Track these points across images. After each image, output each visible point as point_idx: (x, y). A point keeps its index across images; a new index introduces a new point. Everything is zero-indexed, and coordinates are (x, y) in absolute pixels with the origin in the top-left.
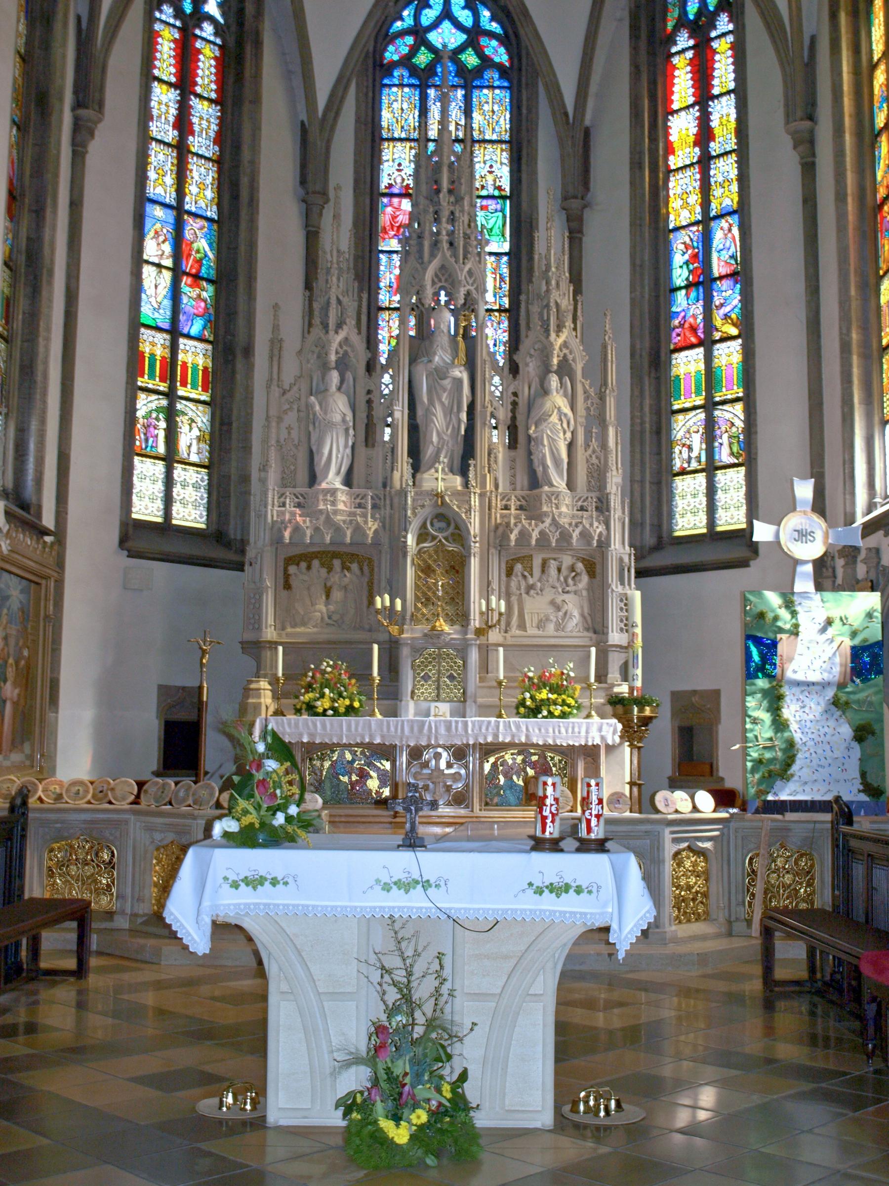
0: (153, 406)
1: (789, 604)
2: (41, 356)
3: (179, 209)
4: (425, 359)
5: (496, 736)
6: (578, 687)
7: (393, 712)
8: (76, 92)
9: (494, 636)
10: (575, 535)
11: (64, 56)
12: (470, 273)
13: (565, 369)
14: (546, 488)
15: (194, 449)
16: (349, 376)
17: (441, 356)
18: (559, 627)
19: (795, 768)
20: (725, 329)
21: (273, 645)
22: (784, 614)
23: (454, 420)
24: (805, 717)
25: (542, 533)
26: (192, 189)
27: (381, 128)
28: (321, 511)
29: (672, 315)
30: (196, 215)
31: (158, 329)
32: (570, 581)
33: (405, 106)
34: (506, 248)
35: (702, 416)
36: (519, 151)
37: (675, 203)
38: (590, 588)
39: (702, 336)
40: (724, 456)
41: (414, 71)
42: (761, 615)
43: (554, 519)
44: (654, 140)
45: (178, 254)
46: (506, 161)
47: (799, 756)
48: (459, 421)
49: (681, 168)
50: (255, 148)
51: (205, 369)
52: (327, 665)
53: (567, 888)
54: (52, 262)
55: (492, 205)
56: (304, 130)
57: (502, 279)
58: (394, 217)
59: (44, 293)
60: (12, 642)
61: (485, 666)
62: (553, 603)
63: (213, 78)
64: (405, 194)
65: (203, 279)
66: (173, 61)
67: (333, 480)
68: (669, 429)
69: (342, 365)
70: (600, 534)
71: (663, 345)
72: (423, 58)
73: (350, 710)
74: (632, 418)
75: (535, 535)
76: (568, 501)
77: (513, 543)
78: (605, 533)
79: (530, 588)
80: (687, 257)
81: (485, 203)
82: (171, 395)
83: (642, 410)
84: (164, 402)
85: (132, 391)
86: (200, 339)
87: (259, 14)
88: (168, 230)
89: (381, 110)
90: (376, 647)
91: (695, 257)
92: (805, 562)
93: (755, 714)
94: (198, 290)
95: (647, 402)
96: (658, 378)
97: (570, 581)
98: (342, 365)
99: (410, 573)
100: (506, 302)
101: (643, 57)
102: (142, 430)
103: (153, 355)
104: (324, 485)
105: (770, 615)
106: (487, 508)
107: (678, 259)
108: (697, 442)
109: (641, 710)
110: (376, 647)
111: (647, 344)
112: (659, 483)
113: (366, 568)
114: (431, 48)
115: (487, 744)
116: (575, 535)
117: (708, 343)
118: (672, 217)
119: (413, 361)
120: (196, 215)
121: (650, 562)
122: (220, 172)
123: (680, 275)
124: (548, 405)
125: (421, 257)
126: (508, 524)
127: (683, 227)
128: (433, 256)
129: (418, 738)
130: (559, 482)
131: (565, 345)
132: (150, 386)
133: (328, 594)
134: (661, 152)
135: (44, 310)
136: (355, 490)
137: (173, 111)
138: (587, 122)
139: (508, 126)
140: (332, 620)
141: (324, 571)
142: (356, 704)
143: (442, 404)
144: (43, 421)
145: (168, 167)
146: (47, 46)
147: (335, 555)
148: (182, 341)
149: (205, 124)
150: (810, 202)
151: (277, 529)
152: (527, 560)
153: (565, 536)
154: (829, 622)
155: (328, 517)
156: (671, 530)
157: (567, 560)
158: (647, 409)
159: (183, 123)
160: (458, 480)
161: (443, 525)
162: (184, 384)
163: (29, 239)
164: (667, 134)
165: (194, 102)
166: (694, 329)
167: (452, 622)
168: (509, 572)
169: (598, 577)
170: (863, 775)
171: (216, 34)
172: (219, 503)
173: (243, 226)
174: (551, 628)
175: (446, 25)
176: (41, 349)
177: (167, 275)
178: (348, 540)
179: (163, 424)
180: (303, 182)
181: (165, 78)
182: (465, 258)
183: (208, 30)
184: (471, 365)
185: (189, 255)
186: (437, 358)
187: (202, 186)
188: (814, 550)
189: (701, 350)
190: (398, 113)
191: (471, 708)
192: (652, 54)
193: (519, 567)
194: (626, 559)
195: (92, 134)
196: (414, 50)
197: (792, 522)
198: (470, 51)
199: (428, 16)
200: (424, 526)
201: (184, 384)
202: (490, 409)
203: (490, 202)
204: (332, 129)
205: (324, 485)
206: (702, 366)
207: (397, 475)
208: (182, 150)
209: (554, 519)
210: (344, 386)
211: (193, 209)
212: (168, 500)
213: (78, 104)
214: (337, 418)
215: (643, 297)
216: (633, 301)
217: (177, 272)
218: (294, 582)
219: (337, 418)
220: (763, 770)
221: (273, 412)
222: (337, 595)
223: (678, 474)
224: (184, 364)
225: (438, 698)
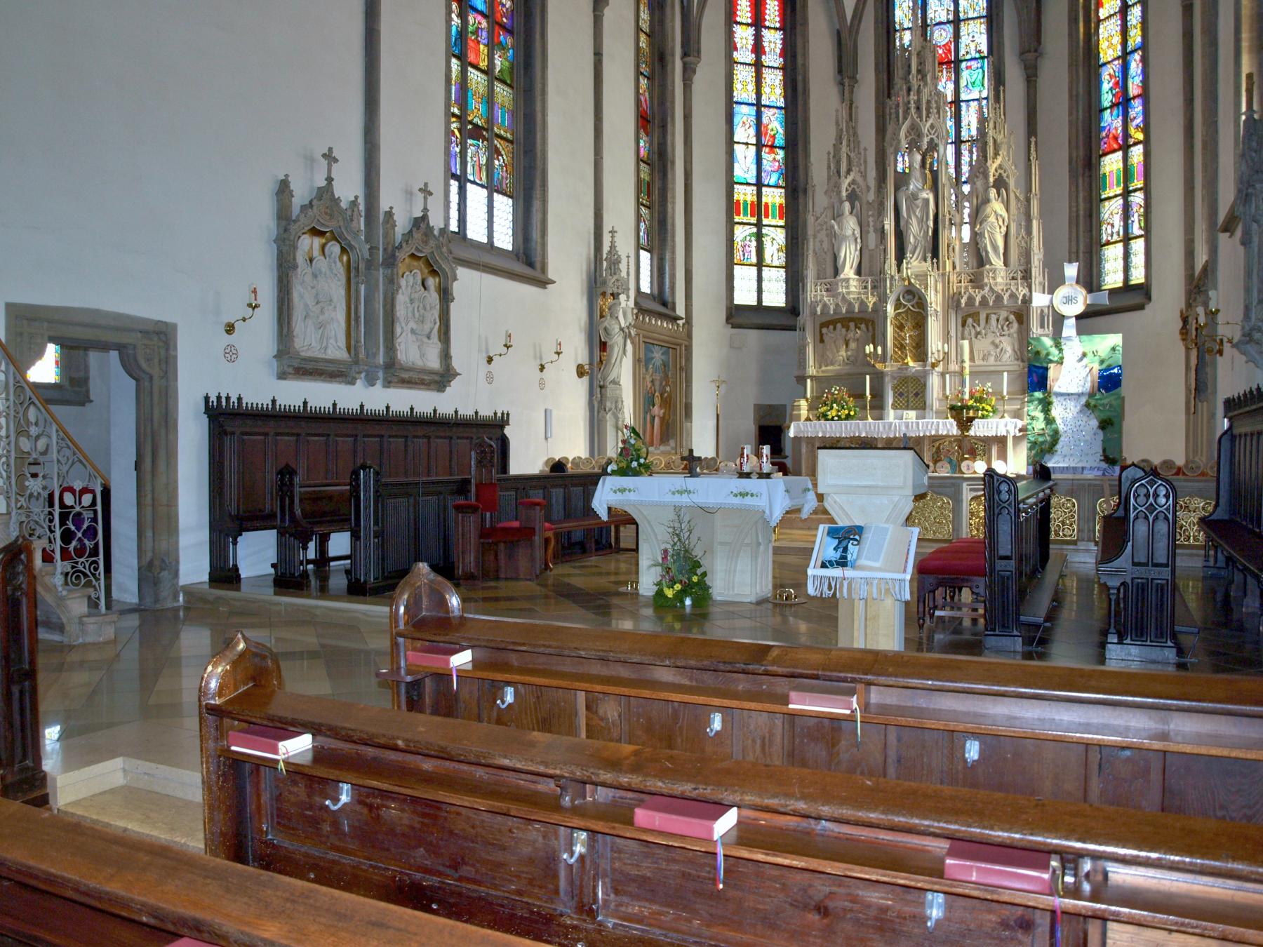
0: (747, 233)
1: (1058, 345)
2: (669, 215)
4: (904, 188)
5: (937, 431)
6: (994, 399)
8: (683, 46)
10: (1006, 297)
11: (673, 27)
12: (932, 126)
13: (1000, 184)
14: (988, 266)
15: (775, 257)
19: (1058, 447)
20: (1136, 136)
22: (1054, 351)
23: (925, 227)
24: (1066, 415)
25: (984, 297)
26: (766, 90)
27: (895, 22)
28: (839, 293)
30: (769, 107)
32: (1005, 328)
35: (1121, 202)
36: (991, 22)
37: (1103, 45)
38: (1020, 332)
39: (1121, 143)
40: (1136, 230)
42: (1038, 353)
43: (991, 287)
46: (984, 31)
47: (1062, 439)
48: (928, 227)
49: (1107, 18)
50: (805, 56)
51: (781, 206)
53: (747, 494)
54: (674, 156)
55: (974, 64)
56: (839, 33)
59: (669, 176)
60: (657, 383)
62: (993, 343)
63: (777, 13)
65: (776, 147)
66: (749, 9)
67: (849, 272)
68: (1099, 213)
69: (852, 197)
70: (1024, 296)
71: (1094, 151)
73: (848, 417)
74: (1070, 208)
75: (978, 299)
76: (1002, 274)
77: (963, 305)
78: (1028, 294)
79: (978, 334)
80: (1111, 84)
81: (969, 64)
82: (759, 225)
85: (731, 225)
86: (777, 186)
89: (894, 10)
90: (868, 377)
91: (1117, 84)
92: (1069, 317)
93: (1033, 414)
94: (773, 155)
96: (1090, 176)
97: (1005, 328)
98: (852, 197)
99: (890, 330)
102: (741, 249)
104: (842, 276)
105: (1044, 353)
107: (1106, 86)
109: (967, 413)
110: (868, 377)
112: (1091, 252)
113: (870, 328)
115: (931, 436)
116: (1006, 297)
117: (1125, 148)
118: (1101, 55)
122: (784, 75)
123: (1107, 99)
124: (988, 210)
125: (898, 121)
126: (960, 293)
127: (1109, 62)
128: (905, 119)
129: (888, 433)
130: (998, 262)
131: (1000, 167)
132: (745, 221)
134: (1093, 7)
135: (670, 186)
136: (863, 278)
139: (985, 5)
141: (844, 330)
142: (852, 413)
143: (917, 217)
144: (673, 253)
145: (749, 79)
146: (662, 22)
147: (851, 320)
148: (764, 189)
149: (772, 45)
150: (1188, 35)
151: (813, 307)
152: (975, 316)
153: (999, 298)
154: (1084, 355)
155: (844, 297)
157: (1003, 314)
158: (1081, 200)
159: (758, 49)
161: (911, 297)
162: (767, 216)
163: (659, 144)
165: (765, 32)
166: (1116, 138)
168: (964, 324)
169: (1025, 324)
170: (1104, 450)
172: (792, 290)
173: (800, 108)
174: (992, 359)
176: (670, 210)
177: (753, 149)
178: (857, 310)
179: (754, 244)
180: (840, 71)
181: (744, 21)
182: (928, 116)
184: (935, 188)
185: (767, 133)
186: (911, 187)
187: (772, 87)
188: (1079, 308)
189: (1120, 154)
193: (970, 321)
194: (1046, 311)
195: (694, 72)
197: (1062, 292)
200: (898, 299)
201: (767, 216)
202: (948, 217)
204: (857, 32)
206: (1121, 165)
208: (758, 66)
209: (991, 287)
210: (855, 211)
211: (768, 103)
213: (685, 54)
214: (849, 232)
215: (1077, 118)
216: (1070, 122)
217: (759, 146)
219: (849, 232)
220: (1037, 448)
222: (853, 345)
223: (1104, 245)
224: (767, 205)
225: (907, 408)
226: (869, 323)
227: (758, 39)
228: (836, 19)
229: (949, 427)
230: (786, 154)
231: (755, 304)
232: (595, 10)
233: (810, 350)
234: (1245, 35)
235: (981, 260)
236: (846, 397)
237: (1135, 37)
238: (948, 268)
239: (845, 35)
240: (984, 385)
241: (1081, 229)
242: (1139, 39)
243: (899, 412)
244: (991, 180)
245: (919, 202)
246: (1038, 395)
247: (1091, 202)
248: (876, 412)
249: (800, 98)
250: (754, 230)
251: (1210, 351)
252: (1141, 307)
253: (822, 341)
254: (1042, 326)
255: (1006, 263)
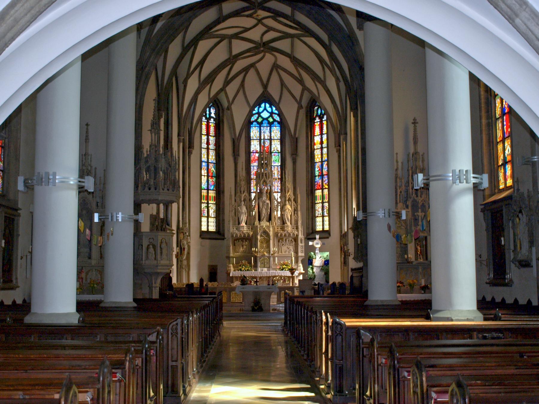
1: (315, 254)
3: (208, 162)
7: (256, 270)
9: (276, 255)
10: (292, 234)
12: (270, 181)
16: (246, 202)
17: (264, 198)
18: (289, 252)
21: (233, 257)
22: (314, 256)
25: (285, 234)
26: (210, 157)
29: (315, 182)
30: (211, 163)
31: (205, 189)
33: (256, 131)
34: (280, 164)
40: (326, 214)
41: (258, 123)
42: (310, 256)
44: (311, 142)
45: (208, 173)
46: (279, 144)
52: (243, 262)
56: (233, 139)
57: (279, 171)
58: (254, 158)
61: (274, 261)
62: (287, 248)
64: (257, 152)
67: (243, 224)
68: (315, 207)
69: (244, 200)
72: (260, 120)
73: (248, 270)
75: (284, 234)
76: (290, 227)
79: (283, 245)
83: (309, 203)
84: (206, 205)
86: (213, 190)
87: (223, 116)
88: (206, 167)
91: (320, 169)
95: (310, 201)
98: (244, 200)
99: (259, 243)
100: (280, 177)
101: (309, 123)
103: (204, 195)
104: (241, 225)
106: (274, 229)
107: (317, 169)
108: (320, 210)
111: (310, 188)
114: (262, 117)
116: (292, 234)
117: (322, 189)
119: (259, 199)
120: (211, 163)
121: (309, 237)
122: (216, 152)
123: (317, 173)
128: (262, 178)
131: (289, 195)
133: (243, 246)
137: (206, 141)
138: (297, 136)
140: (243, 252)
141: (242, 242)
147: (244, 239)
148: (209, 191)
152: (282, 239)
153: (289, 234)
154: (321, 257)
156: (315, 229)
157: (290, 239)
159: (208, 143)
160: (268, 223)
162: (210, 200)
164: (314, 141)
167: (267, 253)
168: (279, 242)
171: (214, 121)
174: (287, 253)
175: (265, 111)
177: (206, 177)
179: (206, 210)
183: (212, 120)
190: (254, 133)
191: (271, 269)
192: (311, 121)
193: (281, 240)
196: (258, 118)
197: (315, 241)
198: (271, 118)
199: (261, 110)
201: (210, 200)
203: (276, 154)
205: (241, 225)
206: (321, 194)
207: (256, 223)
208: (208, 149)
212: (208, 226)
214: (244, 211)
217: (208, 176)
218: (236, 244)
219: (244, 211)
221: (231, 210)
222: (245, 247)
224: (210, 196)
225: (264, 267)
226: (251, 240)
227: (208, 140)
228: (233, 134)
229: (288, 274)
230: (216, 179)
231: (206, 230)
232: (178, 144)
233: (231, 248)
234: (353, 186)
235: (284, 223)
236: (247, 264)
237: (325, 157)
238: (274, 224)
239: (236, 141)
240: (288, 261)
241: (310, 212)
242: (326, 158)
243: (262, 268)
244: (287, 199)
245: (266, 204)
246: (311, 266)
247: (313, 204)
248: (255, 268)
249: (221, 162)
250: (206, 205)
251: (347, 255)
252: (328, 238)
253: (235, 245)
254: (301, 243)
255: (291, 224)
